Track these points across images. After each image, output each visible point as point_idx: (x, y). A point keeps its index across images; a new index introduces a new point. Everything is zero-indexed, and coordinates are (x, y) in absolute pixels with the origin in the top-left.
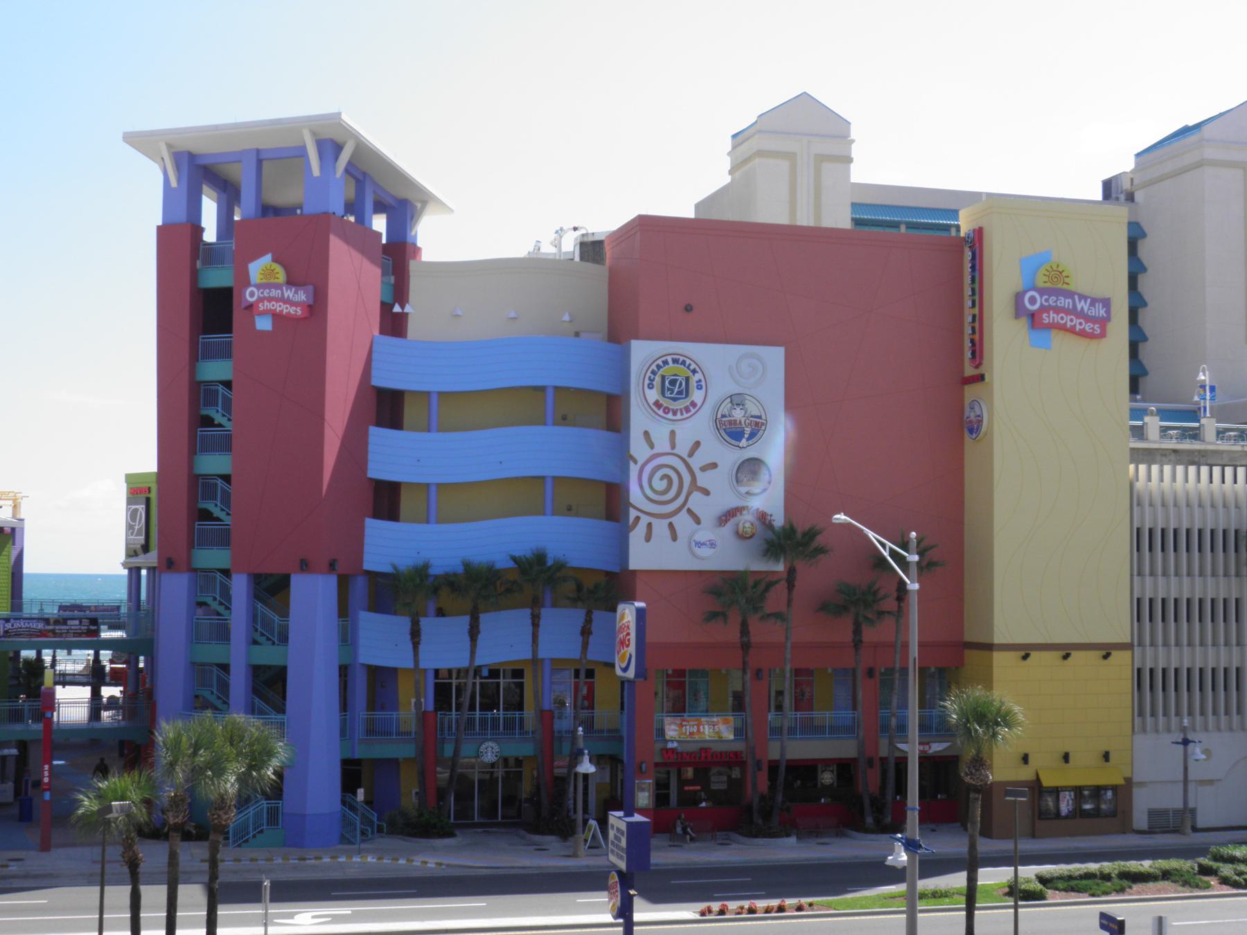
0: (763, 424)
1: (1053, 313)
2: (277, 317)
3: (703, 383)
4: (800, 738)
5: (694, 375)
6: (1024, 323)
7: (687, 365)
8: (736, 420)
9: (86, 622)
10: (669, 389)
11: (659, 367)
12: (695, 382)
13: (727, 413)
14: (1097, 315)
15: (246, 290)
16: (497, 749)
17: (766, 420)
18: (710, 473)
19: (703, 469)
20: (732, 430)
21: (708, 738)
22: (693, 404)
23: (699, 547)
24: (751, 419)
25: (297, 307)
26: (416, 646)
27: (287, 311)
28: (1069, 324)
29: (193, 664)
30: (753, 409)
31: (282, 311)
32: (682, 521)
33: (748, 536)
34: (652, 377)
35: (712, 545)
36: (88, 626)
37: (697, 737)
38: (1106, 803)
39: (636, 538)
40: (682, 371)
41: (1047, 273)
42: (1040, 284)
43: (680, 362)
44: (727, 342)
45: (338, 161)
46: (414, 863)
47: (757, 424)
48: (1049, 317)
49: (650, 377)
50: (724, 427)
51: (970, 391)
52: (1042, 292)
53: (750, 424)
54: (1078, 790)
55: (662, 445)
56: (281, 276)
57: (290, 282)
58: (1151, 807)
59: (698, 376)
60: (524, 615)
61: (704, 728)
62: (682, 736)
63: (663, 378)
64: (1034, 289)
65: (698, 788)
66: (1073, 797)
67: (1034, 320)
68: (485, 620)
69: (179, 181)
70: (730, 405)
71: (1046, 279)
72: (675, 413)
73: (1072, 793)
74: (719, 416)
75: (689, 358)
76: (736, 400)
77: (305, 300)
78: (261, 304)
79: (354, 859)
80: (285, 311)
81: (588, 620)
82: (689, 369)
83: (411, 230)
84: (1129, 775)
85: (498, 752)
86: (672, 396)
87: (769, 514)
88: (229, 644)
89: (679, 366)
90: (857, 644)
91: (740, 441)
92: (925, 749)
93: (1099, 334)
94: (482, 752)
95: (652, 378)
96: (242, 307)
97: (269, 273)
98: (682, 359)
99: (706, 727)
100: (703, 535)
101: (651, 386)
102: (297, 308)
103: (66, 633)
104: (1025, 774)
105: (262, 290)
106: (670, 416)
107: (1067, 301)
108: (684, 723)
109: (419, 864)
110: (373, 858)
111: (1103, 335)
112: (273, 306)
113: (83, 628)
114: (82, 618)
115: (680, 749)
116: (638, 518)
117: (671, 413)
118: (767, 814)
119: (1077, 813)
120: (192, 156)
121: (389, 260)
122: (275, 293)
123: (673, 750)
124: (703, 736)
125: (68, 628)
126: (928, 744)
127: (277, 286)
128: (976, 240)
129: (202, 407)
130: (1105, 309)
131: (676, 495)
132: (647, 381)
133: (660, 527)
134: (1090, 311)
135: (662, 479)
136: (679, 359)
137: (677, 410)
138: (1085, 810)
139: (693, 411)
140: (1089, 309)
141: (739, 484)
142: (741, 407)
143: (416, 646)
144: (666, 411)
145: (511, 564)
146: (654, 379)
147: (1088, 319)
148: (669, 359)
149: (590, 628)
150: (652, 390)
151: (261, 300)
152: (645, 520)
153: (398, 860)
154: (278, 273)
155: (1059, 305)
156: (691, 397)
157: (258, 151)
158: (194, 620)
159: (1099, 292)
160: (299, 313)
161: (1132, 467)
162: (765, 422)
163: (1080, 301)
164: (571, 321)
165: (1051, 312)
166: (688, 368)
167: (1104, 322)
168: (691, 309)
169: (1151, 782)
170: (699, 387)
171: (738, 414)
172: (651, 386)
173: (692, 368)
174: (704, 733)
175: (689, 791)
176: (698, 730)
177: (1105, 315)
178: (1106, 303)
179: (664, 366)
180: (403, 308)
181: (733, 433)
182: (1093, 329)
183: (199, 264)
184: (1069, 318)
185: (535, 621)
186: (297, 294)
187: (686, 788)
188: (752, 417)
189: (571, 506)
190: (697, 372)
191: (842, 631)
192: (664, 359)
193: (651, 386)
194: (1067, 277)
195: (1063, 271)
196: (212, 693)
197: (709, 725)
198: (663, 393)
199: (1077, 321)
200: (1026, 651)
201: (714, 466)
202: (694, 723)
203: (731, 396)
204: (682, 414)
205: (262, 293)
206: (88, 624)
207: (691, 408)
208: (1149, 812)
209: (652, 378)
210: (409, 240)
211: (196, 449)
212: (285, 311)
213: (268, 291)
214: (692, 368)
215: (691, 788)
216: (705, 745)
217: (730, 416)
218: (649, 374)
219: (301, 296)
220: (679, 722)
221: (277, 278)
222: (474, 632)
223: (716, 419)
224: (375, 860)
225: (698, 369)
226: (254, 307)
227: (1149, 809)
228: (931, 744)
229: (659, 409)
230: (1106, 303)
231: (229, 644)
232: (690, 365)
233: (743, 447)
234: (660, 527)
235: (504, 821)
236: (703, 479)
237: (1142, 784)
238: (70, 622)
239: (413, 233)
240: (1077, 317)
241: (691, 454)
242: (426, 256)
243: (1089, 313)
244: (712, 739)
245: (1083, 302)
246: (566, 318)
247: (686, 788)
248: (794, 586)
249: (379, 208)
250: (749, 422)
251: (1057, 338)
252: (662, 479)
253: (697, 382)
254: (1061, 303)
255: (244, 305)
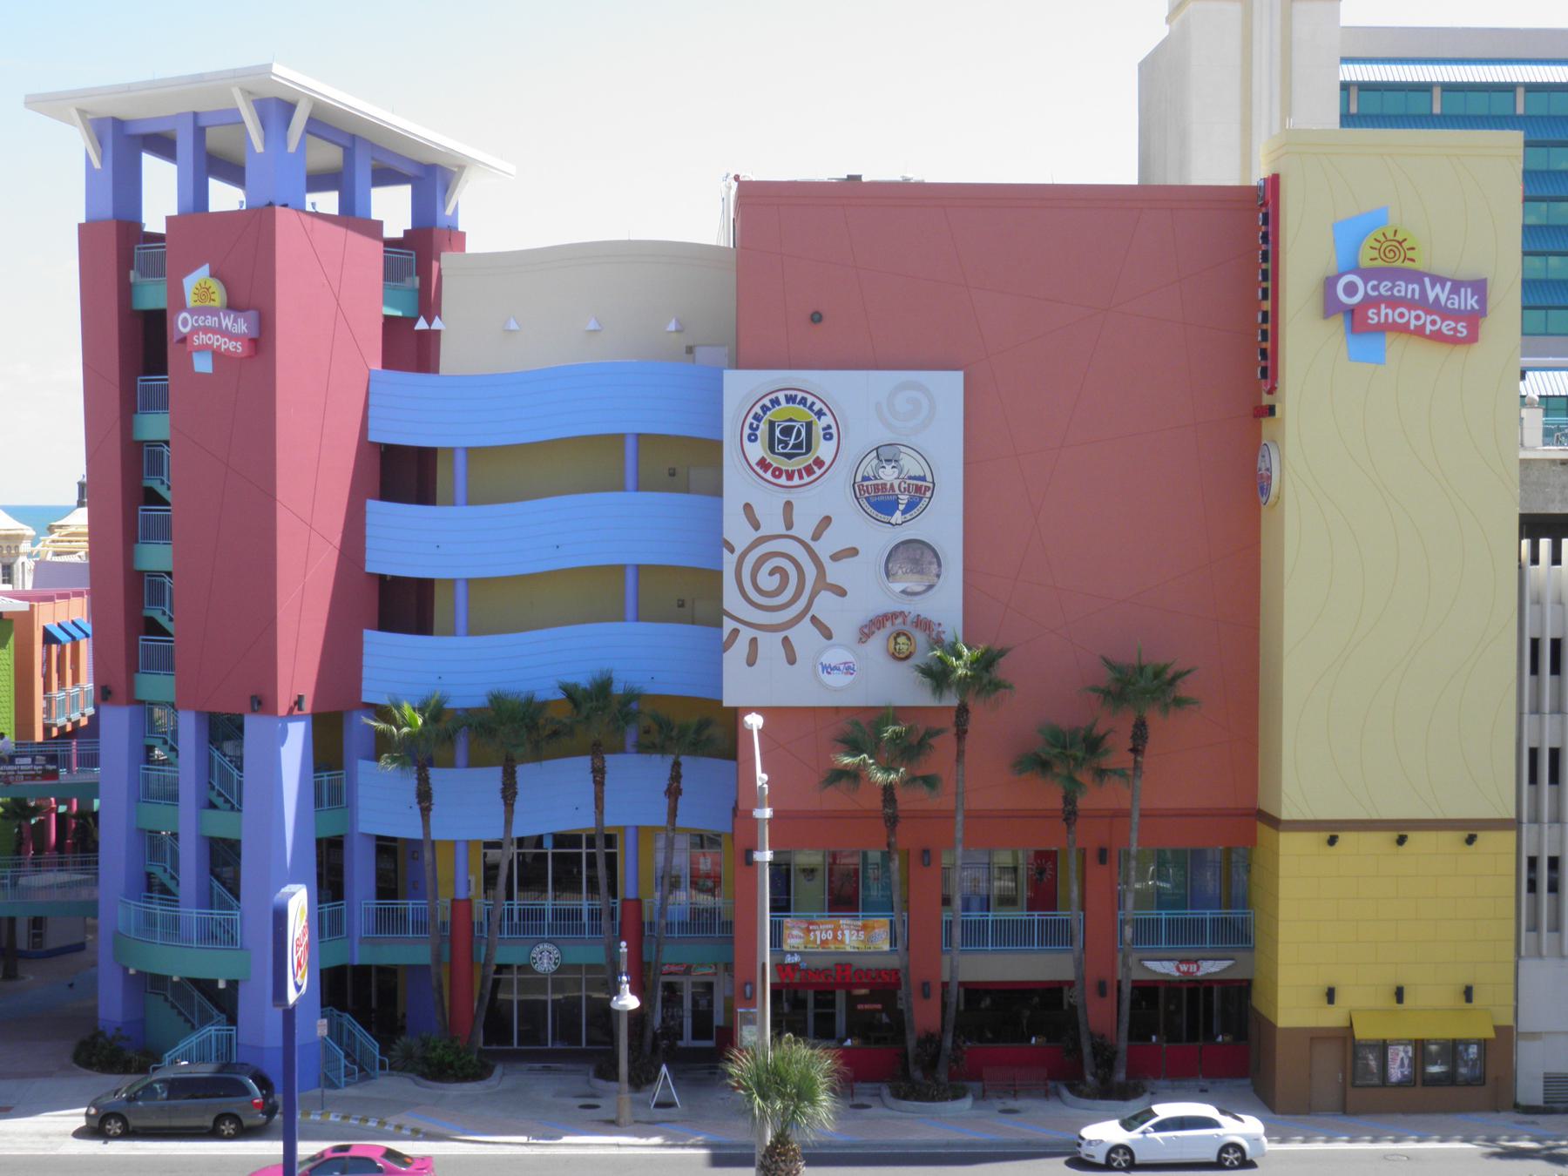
0: (927, 488)
1: (1386, 308)
2: (217, 355)
3: (834, 431)
4: (993, 950)
5: (819, 418)
6: (1338, 324)
7: (808, 404)
8: (885, 484)
9: (40, 759)
10: (780, 441)
11: (765, 409)
12: (821, 430)
13: (871, 474)
14: (1463, 307)
15: (179, 315)
16: (556, 954)
17: (933, 483)
18: (846, 563)
19: (835, 557)
20: (882, 498)
21: (849, 949)
22: (819, 463)
23: (829, 673)
24: (908, 481)
25: (236, 341)
26: (425, 812)
27: (226, 347)
28: (1413, 323)
29: (142, 831)
30: (912, 466)
31: (219, 347)
32: (804, 635)
33: (902, 656)
34: (755, 423)
35: (849, 669)
36: (43, 765)
37: (832, 947)
38: (1466, 1065)
39: (734, 659)
40: (801, 414)
41: (1377, 245)
42: (1365, 262)
43: (798, 399)
44: (877, 367)
45: (290, 129)
46: (386, 1128)
47: (918, 489)
48: (1378, 314)
49: (751, 424)
50: (867, 495)
51: (1266, 422)
52: (1366, 275)
53: (907, 489)
54: (1420, 1046)
55: (772, 522)
56: (218, 296)
57: (233, 306)
58: (1547, 1070)
59: (827, 420)
60: (585, 762)
61: (843, 934)
62: (809, 946)
63: (772, 424)
64: (1357, 270)
65: (879, 1006)
66: (1410, 1054)
67: (1356, 320)
68: (524, 772)
69: (102, 161)
70: (876, 461)
71: (1375, 254)
72: (790, 477)
73: (1410, 1049)
74: (859, 479)
75: (812, 394)
76: (885, 453)
77: (246, 331)
78: (196, 336)
79: (312, 1117)
80: (223, 347)
81: (676, 776)
82: (812, 411)
83: (445, 207)
84: (1506, 1020)
85: (558, 958)
86: (785, 451)
87: (937, 622)
88: (177, 805)
89: (796, 406)
90: (1070, 815)
91: (892, 514)
92: (1191, 970)
93: (1466, 337)
94: (534, 958)
95: (755, 426)
96: (175, 340)
97: (204, 292)
98: (800, 395)
99: (847, 933)
100: (835, 656)
101: (753, 438)
102: (236, 342)
103: (14, 775)
104: (1331, 1018)
105: (196, 317)
106: (783, 480)
107: (1410, 287)
108: (811, 927)
109: (392, 1129)
110: (337, 1116)
111: (1472, 338)
112: (210, 339)
113: (36, 768)
114: (35, 755)
115: (803, 965)
116: (735, 632)
117: (784, 476)
118: (930, 1066)
119: (1418, 1079)
120: (118, 124)
121: (411, 255)
122: (211, 321)
123: (795, 966)
124: (842, 946)
125: (15, 768)
126: (1196, 961)
127: (213, 312)
128: (1269, 197)
129: (145, 476)
130: (1476, 297)
131: (790, 600)
132: (747, 431)
133: (770, 645)
134: (1450, 302)
135: (771, 573)
136: (796, 396)
137: (793, 472)
138: (1433, 1075)
139: (818, 472)
140: (1448, 299)
141: (891, 579)
142: (893, 464)
143: (425, 812)
144: (777, 473)
145: (560, 695)
146: (758, 427)
147: (1446, 314)
148: (781, 396)
149: (678, 787)
150: (754, 444)
151: (195, 331)
152: (746, 634)
153: (367, 1121)
154: (213, 293)
155: (207, 324)
156: (816, 449)
157: (196, 115)
158: (141, 771)
159: (1467, 269)
160: (240, 350)
161: (1526, 543)
162: (931, 485)
163: (1433, 287)
164: (677, 331)
165: (1383, 306)
166: (811, 408)
167: (1473, 319)
168: (820, 319)
169: (1546, 1033)
170: (828, 437)
171: (888, 475)
172: (753, 437)
173: (816, 408)
174: (842, 942)
175: (864, 1011)
176: (835, 937)
177: (1476, 307)
178: (1479, 288)
179: (774, 407)
180: (430, 322)
181: (881, 503)
182: (1455, 329)
183: (133, 276)
184: (1413, 313)
185: (599, 774)
186: (237, 323)
187: (860, 1007)
188: (910, 478)
189: (683, 601)
190: (825, 414)
191: (1049, 795)
192: (773, 396)
193: (753, 437)
194: (1413, 249)
195: (1405, 240)
196: (165, 870)
197: (851, 930)
198: (772, 448)
199: (1426, 319)
200: (1332, 831)
201: (853, 552)
202: (828, 926)
203: (877, 449)
204: (801, 477)
205: (197, 321)
206: (44, 763)
207: (815, 468)
208: (1545, 1078)
209: (755, 426)
210: (441, 222)
211: (137, 532)
212: (223, 347)
213: (203, 318)
214: (816, 408)
215: (867, 1007)
216: (844, 960)
217: (876, 479)
218: (750, 420)
219: (240, 325)
220: (804, 926)
221: (213, 300)
222: (509, 792)
223: (855, 483)
224: (338, 1119)
225: (825, 410)
226: (188, 341)
227: (1545, 1074)
228: (1199, 962)
229: (766, 471)
230: (1479, 288)
231: (177, 805)
232: (813, 404)
233: (896, 524)
234: (770, 645)
235: (589, 1047)
236: (835, 572)
237: (1534, 1036)
238: (18, 761)
239: (449, 212)
240: (1428, 312)
241: (816, 537)
242: (474, 245)
243: (1449, 305)
244: (857, 950)
245: (1438, 288)
246: (672, 326)
247: (860, 1007)
248: (965, 732)
249: (386, 176)
250: (906, 486)
251: (1395, 346)
252: (771, 573)
253: (824, 429)
254: (1399, 291)
255: (176, 338)
